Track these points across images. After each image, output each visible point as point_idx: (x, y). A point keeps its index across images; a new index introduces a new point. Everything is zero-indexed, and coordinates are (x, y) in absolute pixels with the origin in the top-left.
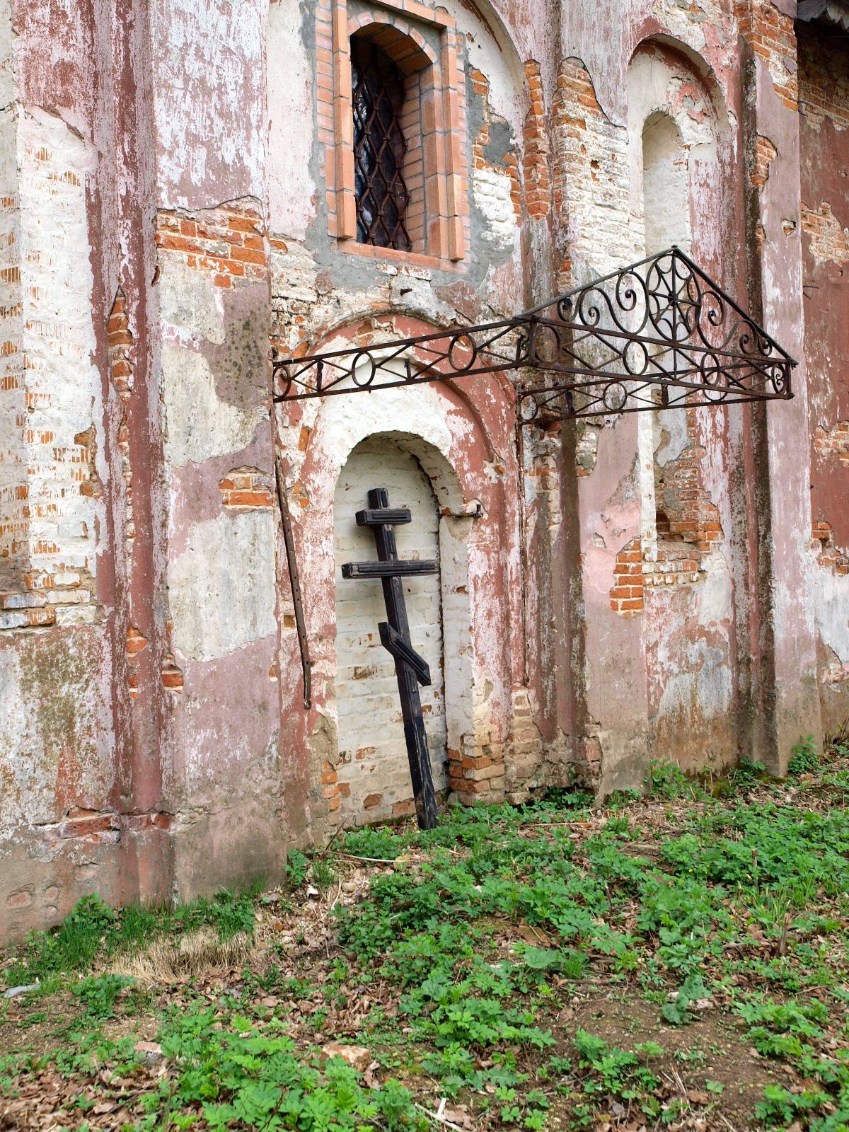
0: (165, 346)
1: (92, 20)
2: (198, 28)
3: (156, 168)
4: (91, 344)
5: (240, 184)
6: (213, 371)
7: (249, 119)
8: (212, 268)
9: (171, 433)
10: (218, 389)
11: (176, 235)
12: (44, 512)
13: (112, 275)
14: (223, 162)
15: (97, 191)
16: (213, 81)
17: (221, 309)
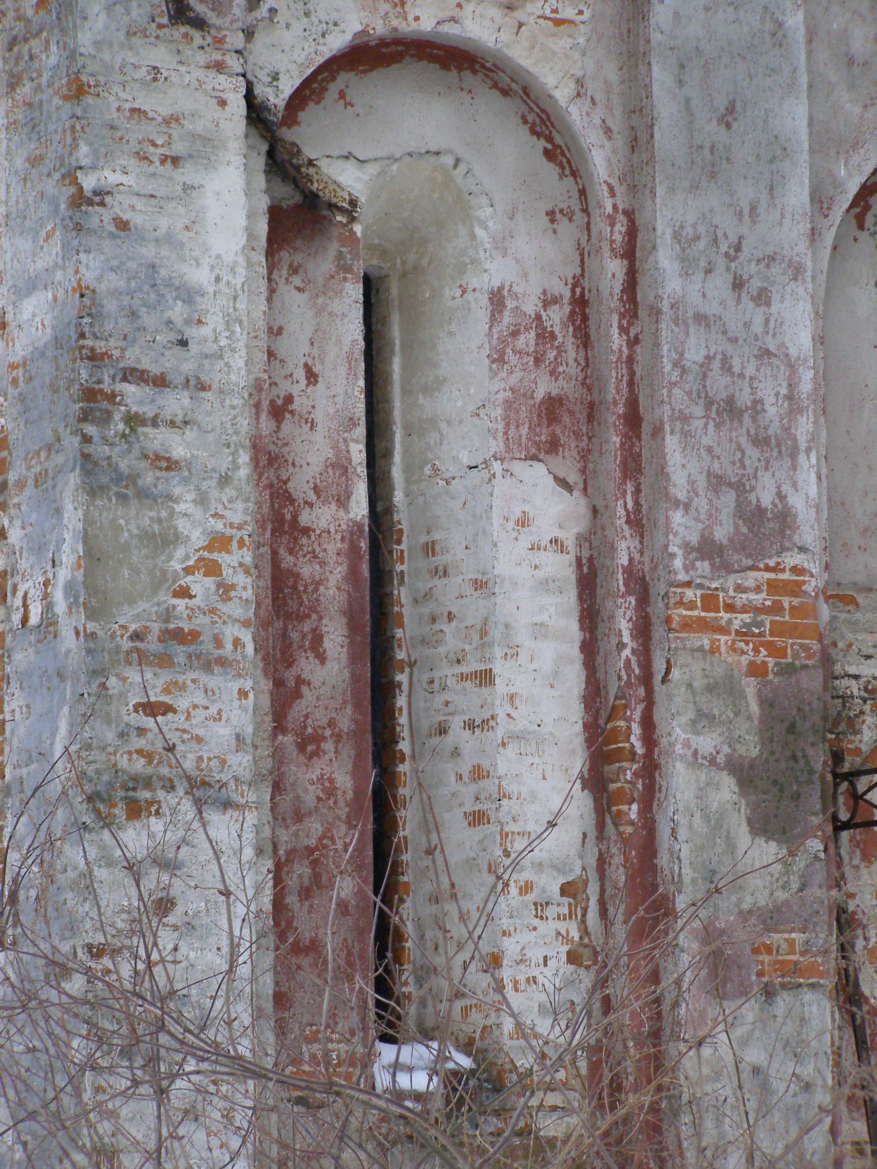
0: (678, 764)
1: (587, 336)
2: (725, 333)
3: (668, 529)
4: (578, 762)
5: (782, 531)
6: (743, 793)
7: (795, 440)
8: (743, 653)
9: (687, 880)
10: (750, 822)
11: (695, 613)
12: (522, 987)
13: (611, 671)
14: (759, 507)
15: (591, 559)
16: (744, 398)
17: (754, 708)
